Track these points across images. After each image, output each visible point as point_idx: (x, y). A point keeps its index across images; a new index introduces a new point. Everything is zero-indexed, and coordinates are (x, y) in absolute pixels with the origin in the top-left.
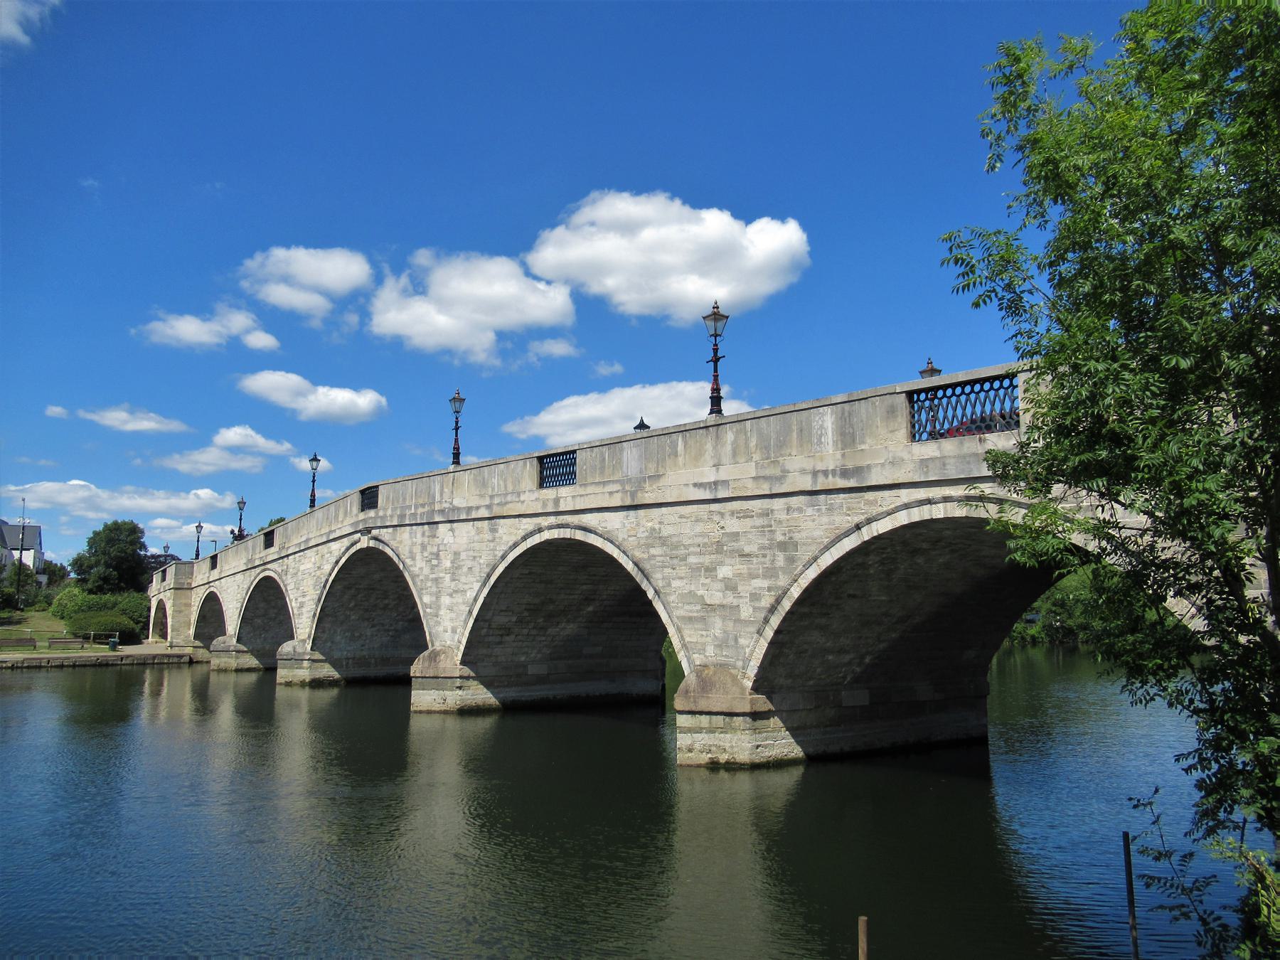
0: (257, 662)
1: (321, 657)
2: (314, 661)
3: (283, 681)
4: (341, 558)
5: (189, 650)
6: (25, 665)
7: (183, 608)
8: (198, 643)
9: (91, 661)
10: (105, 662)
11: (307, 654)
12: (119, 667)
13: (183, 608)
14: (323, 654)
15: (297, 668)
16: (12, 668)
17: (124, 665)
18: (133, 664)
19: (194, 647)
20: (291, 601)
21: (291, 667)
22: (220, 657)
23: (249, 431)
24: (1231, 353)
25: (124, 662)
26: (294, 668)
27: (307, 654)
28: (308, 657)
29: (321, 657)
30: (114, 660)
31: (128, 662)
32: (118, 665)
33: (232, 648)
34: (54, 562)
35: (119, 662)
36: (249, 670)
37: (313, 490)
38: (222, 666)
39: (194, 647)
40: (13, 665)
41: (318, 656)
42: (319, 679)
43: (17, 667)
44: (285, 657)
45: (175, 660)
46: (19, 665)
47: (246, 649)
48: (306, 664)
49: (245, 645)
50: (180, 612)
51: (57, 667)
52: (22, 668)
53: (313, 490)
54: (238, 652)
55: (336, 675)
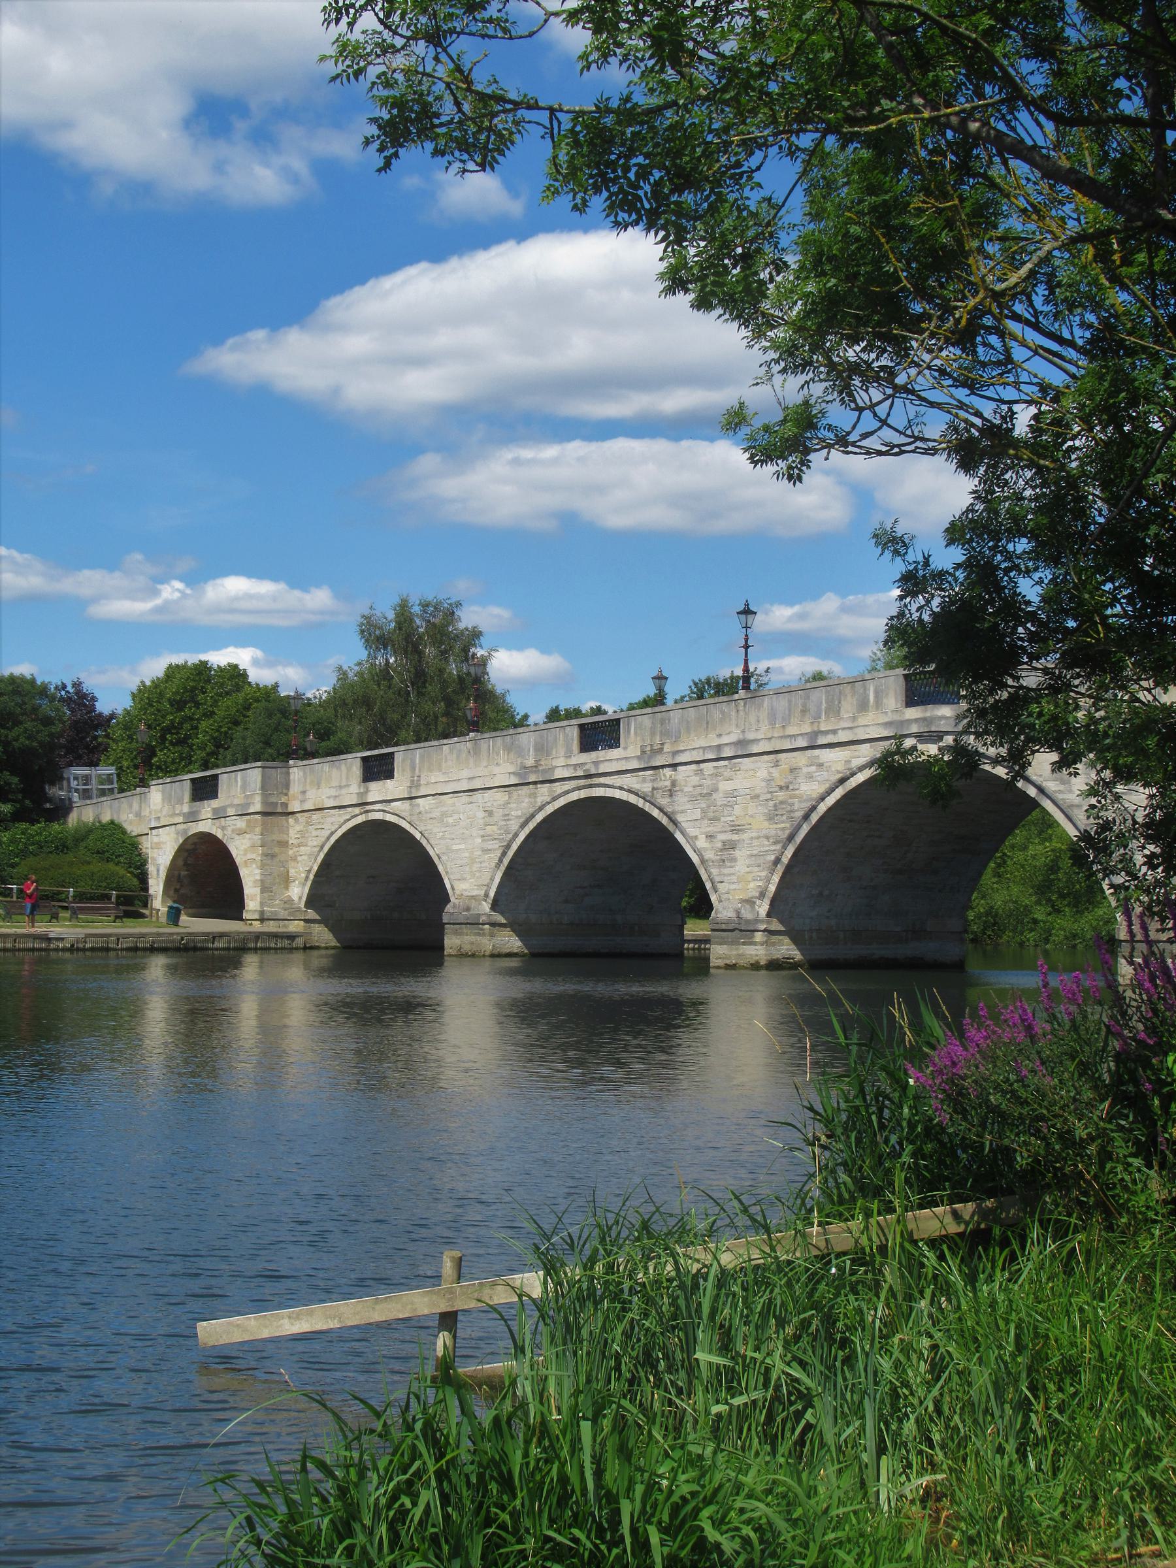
0: (520, 943)
1: (780, 927)
2: (772, 933)
3: (720, 963)
4: (853, 774)
5: (295, 927)
6: (88, 946)
7: (277, 850)
8: (312, 914)
9: (173, 941)
10: (192, 945)
11: (762, 921)
12: (210, 952)
13: (277, 850)
14: (781, 922)
15: (744, 944)
16: (72, 949)
17: (217, 949)
18: (228, 949)
19: (306, 921)
20: (692, 840)
21: (734, 943)
22: (461, 934)
23: (281, 586)
24: (1059, 749)
25: (216, 945)
26: (738, 944)
27: (762, 921)
28: (762, 927)
29: (780, 927)
30: (205, 941)
31: (221, 945)
32: (207, 949)
33: (483, 919)
34: (241, 667)
35: (210, 945)
36: (510, 955)
37: (746, 662)
38: (467, 948)
39: (306, 921)
40: (72, 946)
41: (776, 926)
42: (778, 959)
43: (78, 949)
44: (724, 927)
45: (285, 943)
46: (81, 946)
47: (503, 921)
48: (759, 937)
49: (502, 914)
50: (273, 856)
51: (128, 949)
52: (84, 950)
53: (746, 662)
54: (493, 925)
55: (797, 955)
